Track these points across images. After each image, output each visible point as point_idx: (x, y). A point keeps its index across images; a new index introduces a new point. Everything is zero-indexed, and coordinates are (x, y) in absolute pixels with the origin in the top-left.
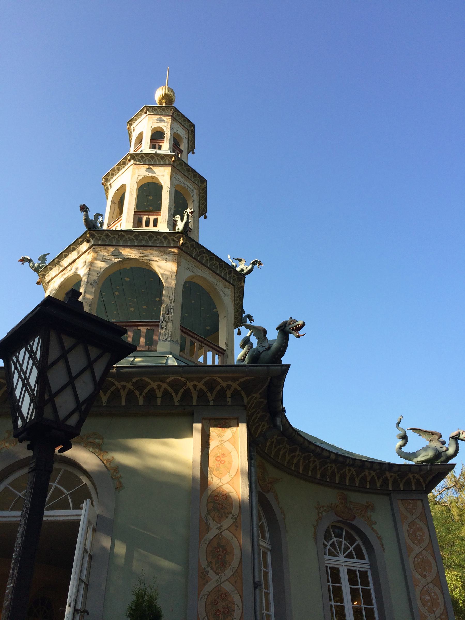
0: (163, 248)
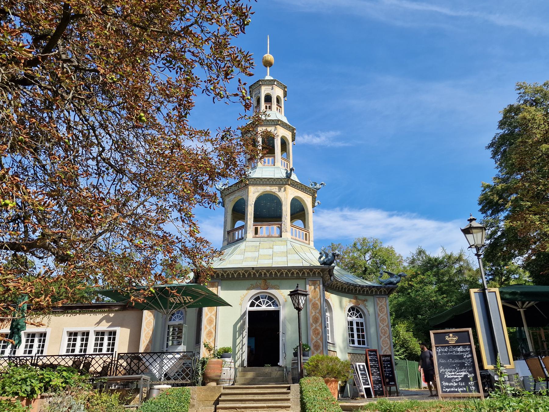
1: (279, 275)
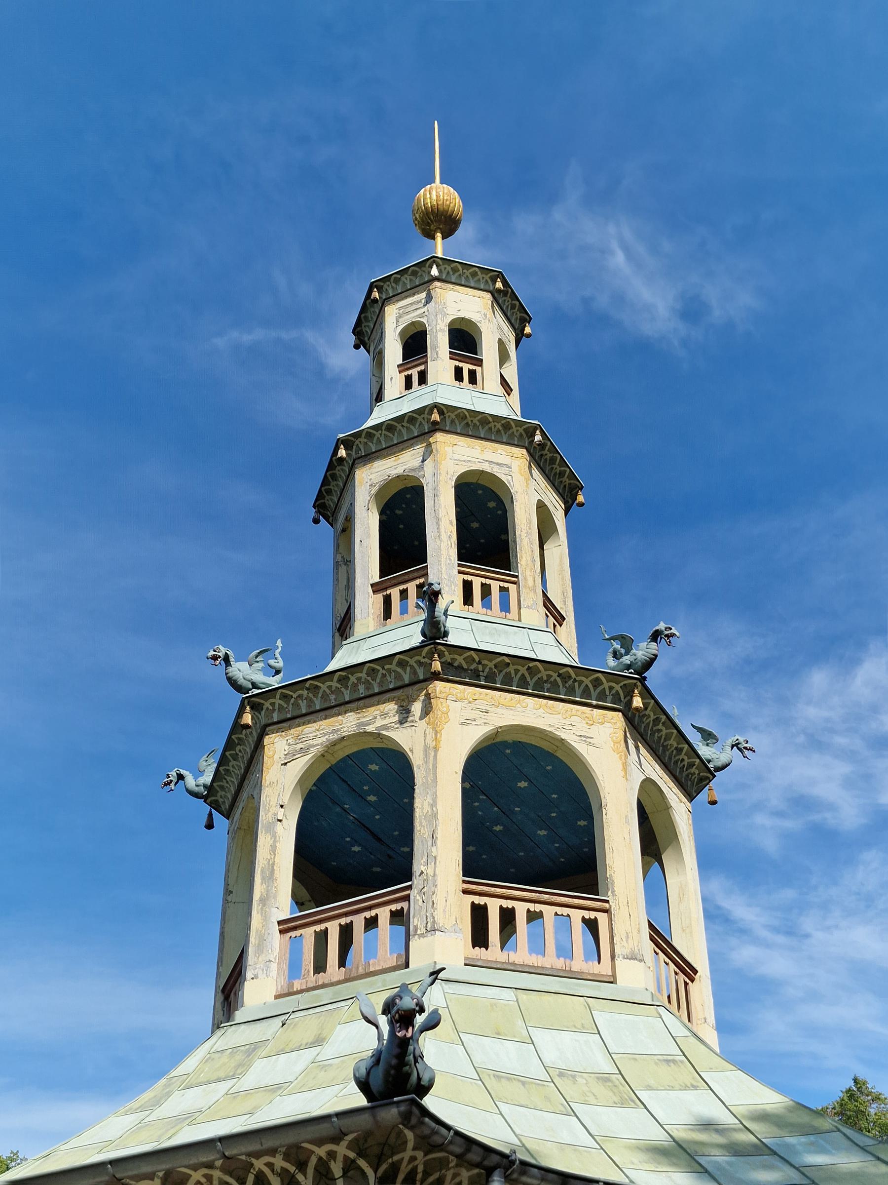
0: (406, 689)
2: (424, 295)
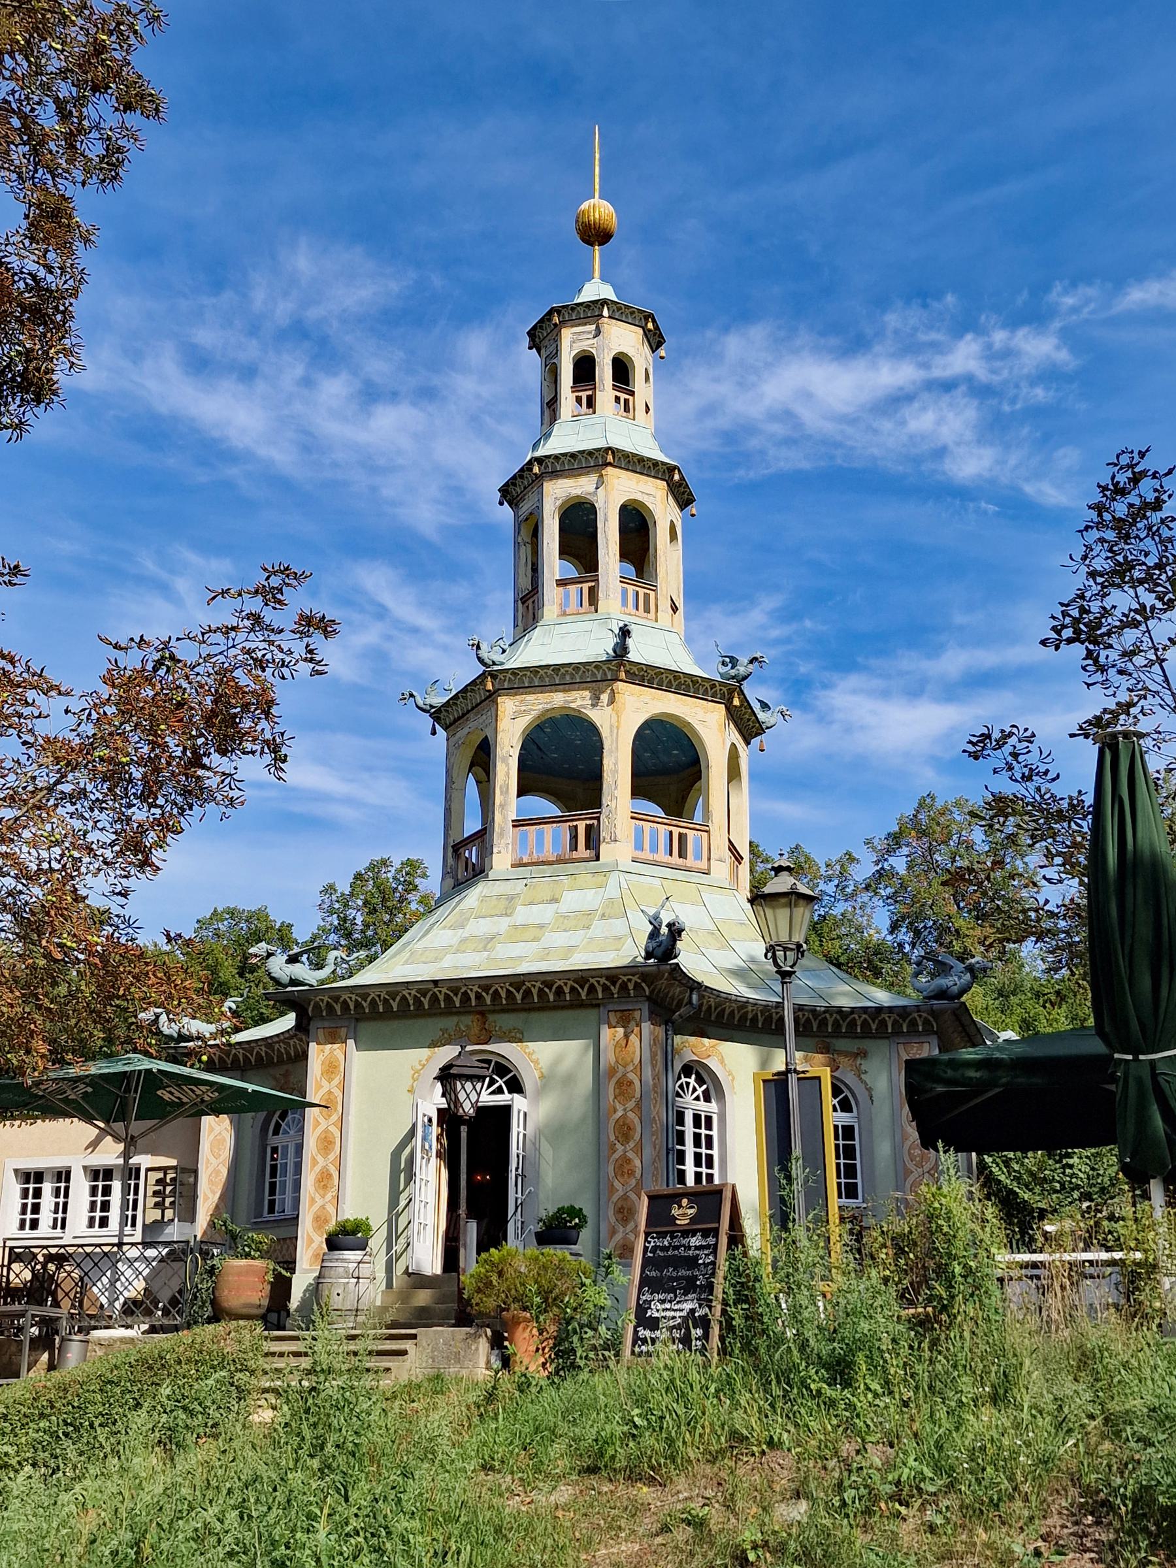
1: (519, 997)
2: (593, 327)
